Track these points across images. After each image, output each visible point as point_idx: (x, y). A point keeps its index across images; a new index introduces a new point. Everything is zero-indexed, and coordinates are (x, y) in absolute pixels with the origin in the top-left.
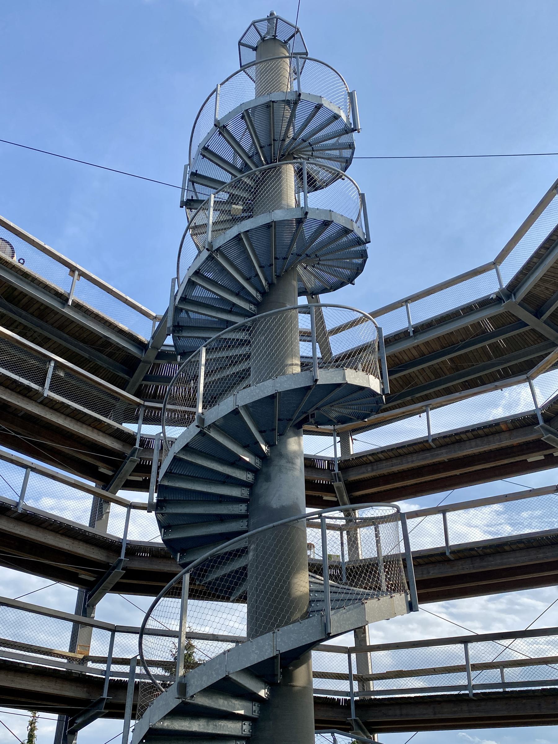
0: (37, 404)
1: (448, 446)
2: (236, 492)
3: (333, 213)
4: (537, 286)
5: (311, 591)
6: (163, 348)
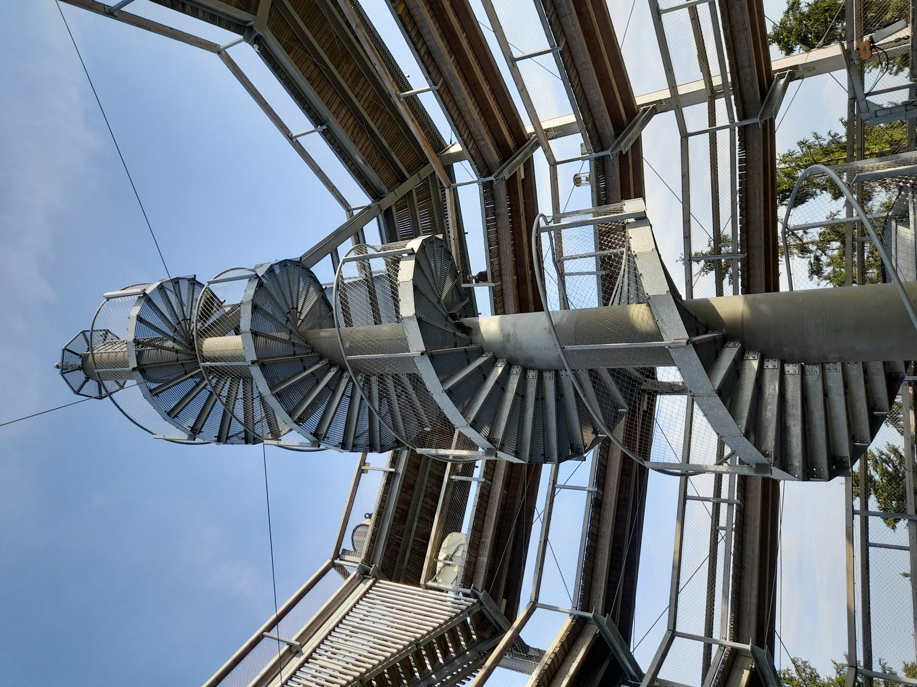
0: (493, 483)
1: (437, 64)
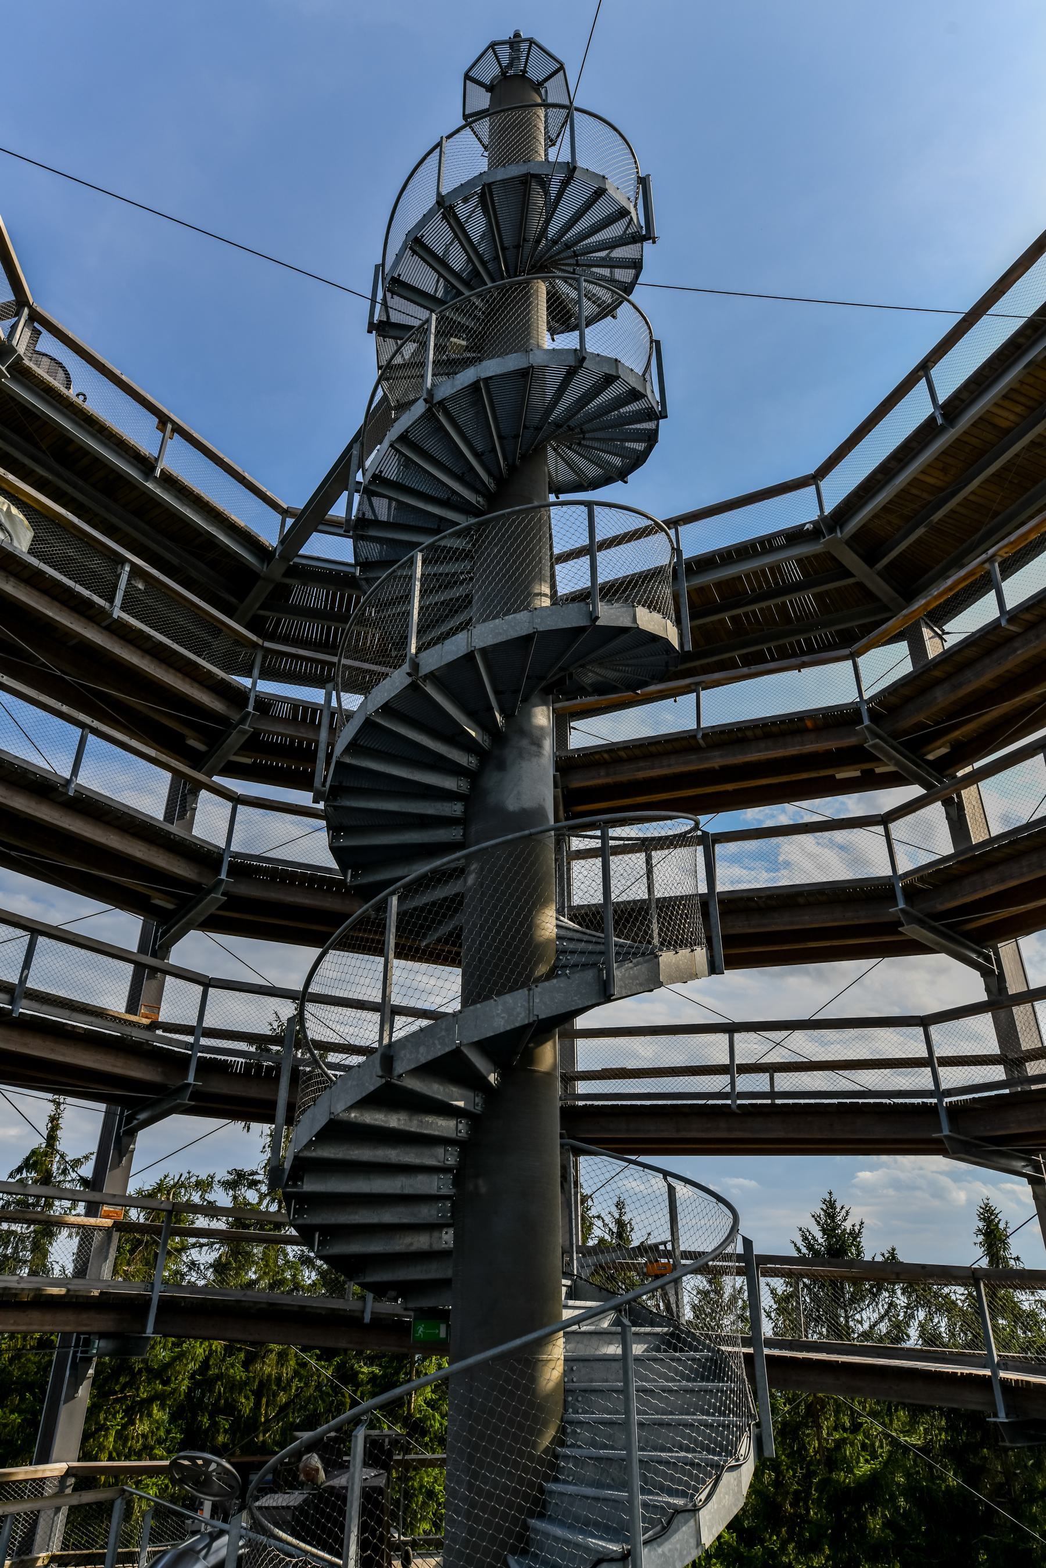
2: (449, 783)
3: (619, 365)
4: (876, 516)
5: (559, 938)
6: (296, 560)
